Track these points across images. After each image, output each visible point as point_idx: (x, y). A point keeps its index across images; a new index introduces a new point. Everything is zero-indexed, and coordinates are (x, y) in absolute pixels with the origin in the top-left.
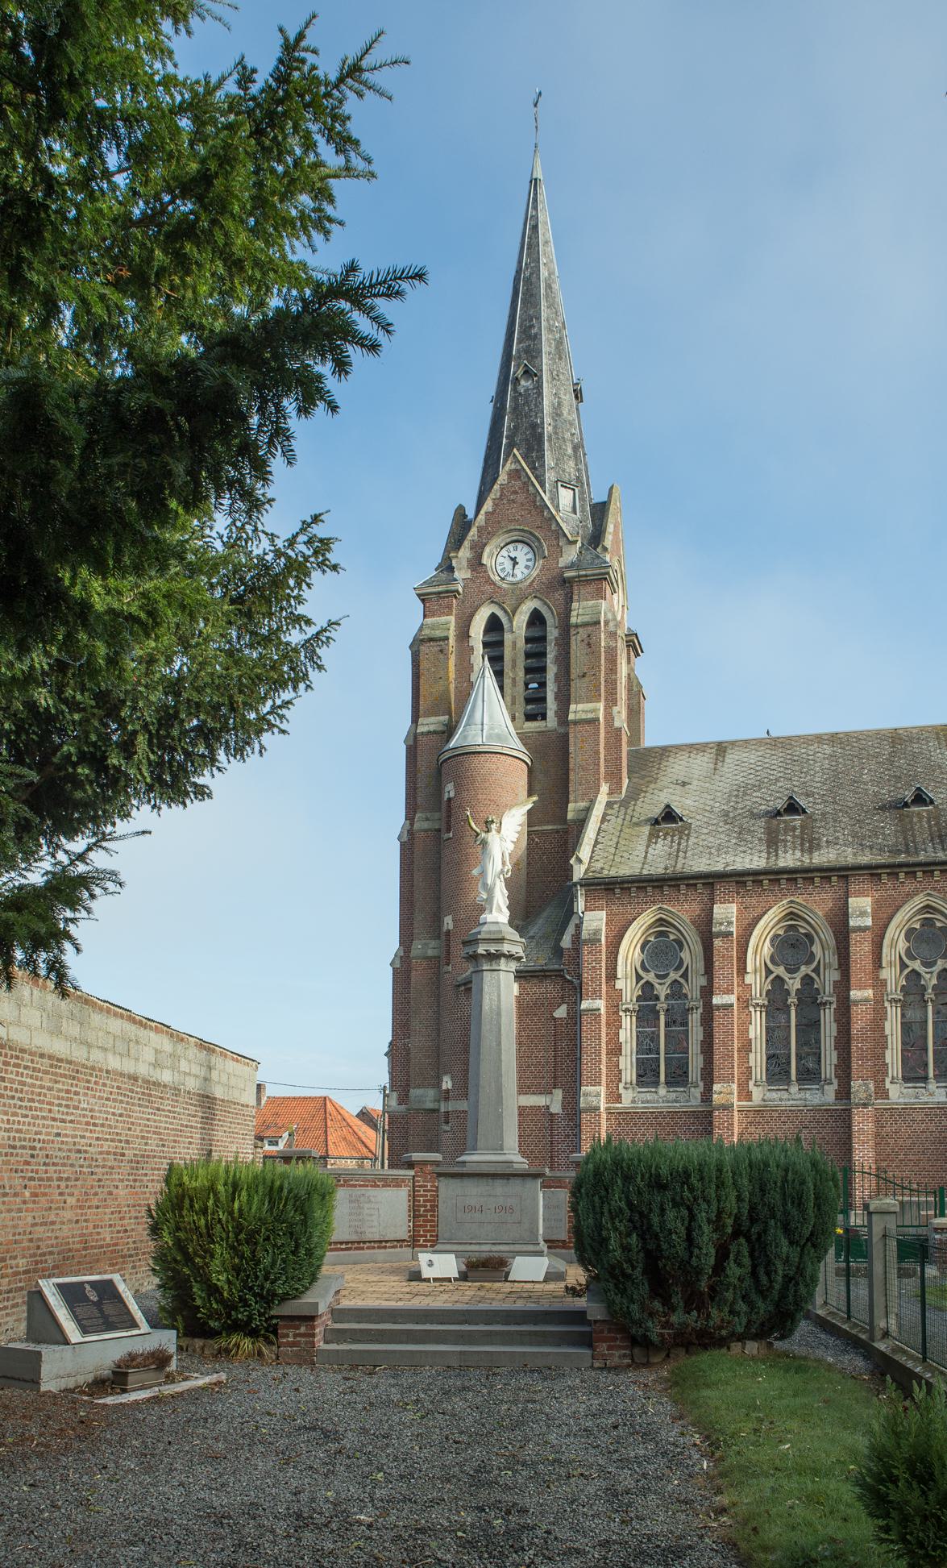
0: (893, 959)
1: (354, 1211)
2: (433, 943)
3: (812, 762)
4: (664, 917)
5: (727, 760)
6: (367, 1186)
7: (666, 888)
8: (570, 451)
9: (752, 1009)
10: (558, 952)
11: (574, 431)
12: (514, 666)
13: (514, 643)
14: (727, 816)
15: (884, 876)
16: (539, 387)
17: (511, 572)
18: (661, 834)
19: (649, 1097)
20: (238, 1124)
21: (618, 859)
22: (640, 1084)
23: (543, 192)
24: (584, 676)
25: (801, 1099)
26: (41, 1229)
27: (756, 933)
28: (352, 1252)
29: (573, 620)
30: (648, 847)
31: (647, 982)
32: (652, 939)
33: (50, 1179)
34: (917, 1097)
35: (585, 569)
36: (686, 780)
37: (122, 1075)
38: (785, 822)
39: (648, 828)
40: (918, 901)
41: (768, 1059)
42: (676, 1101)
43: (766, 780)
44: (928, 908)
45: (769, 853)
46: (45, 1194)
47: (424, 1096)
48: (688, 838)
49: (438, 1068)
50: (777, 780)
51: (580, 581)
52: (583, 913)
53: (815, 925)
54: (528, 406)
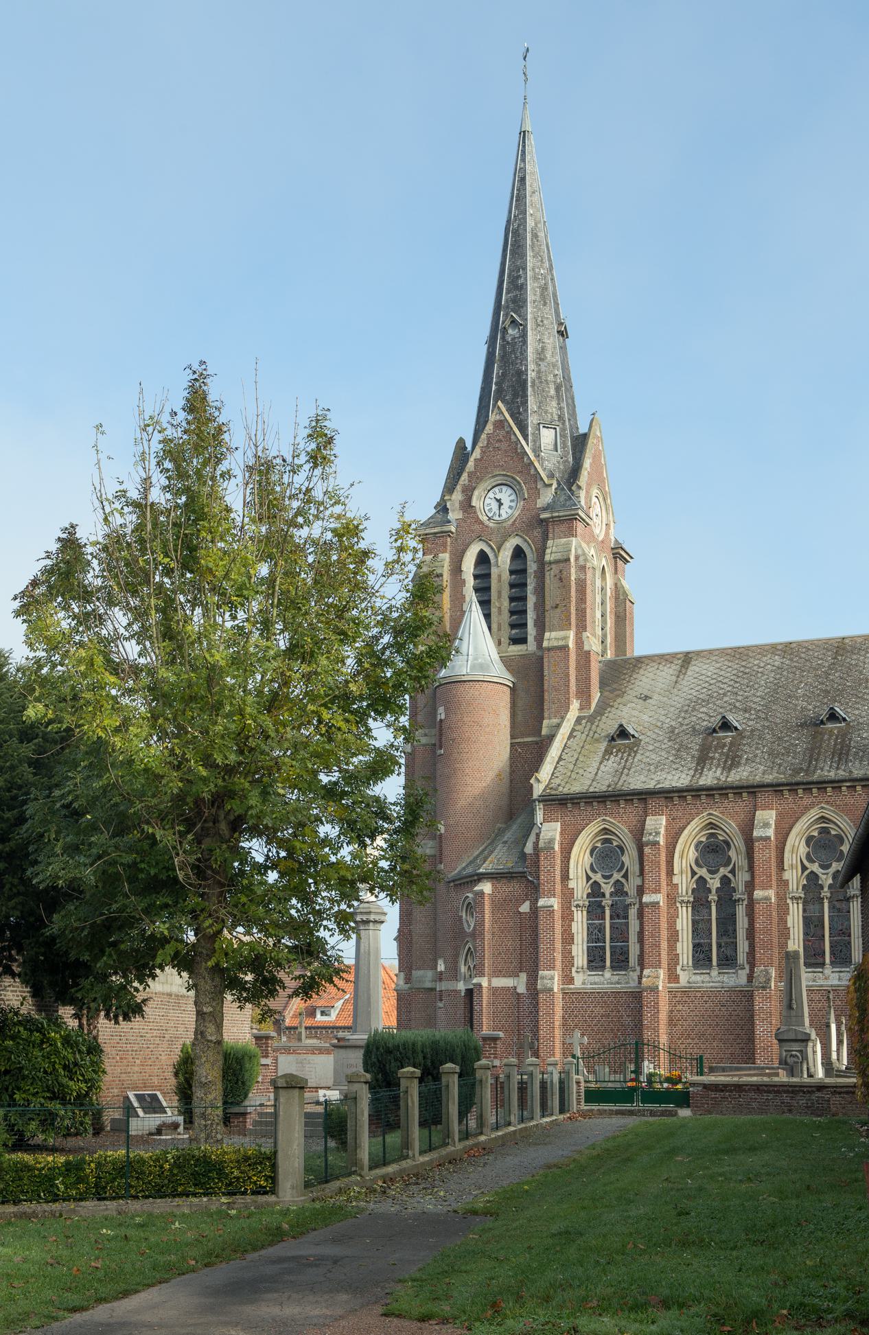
0: (794, 862)
3: (759, 675)
4: (608, 827)
5: (689, 673)
7: (608, 803)
8: (552, 392)
9: (678, 905)
10: (523, 856)
11: (556, 372)
12: (499, 597)
13: (500, 576)
14: (673, 732)
15: (786, 793)
16: (524, 335)
17: (497, 512)
18: (615, 750)
19: (597, 979)
21: (573, 777)
22: (590, 968)
23: (531, 141)
24: (556, 607)
25: (719, 982)
26: (124, 1075)
27: (681, 840)
29: (547, 558)
30: (601, 763)
31: (595, 882)
32: (599, 845)
33: (128, 1051)
34: (814, 981)
35: (558, 511)
36: (649, 694)
37: (163, 994)
38: (719, 738)
39: (605, 744)
40: (814, 813)
41: (694, 947)
42: (618, 983)
43: (715, 694)
44: (823, 819)
45: (696, 770)
46: (126, 1058)
47: (425, 977)
48: (635, 755)
50: (725, 694)
51: (554, 521)
52: (541, 824)
53: (730, 834)
54: (515, 354)
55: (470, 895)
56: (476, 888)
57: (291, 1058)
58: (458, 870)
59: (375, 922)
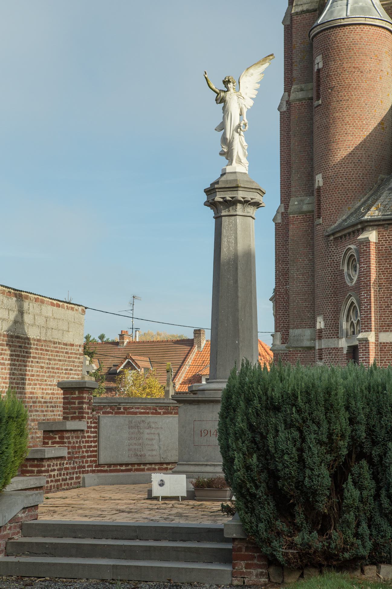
1: (133, 436)
2: (308, 199)
6: (148, 413)
20: (60, 360)
28: (132, 473)
49: (314, 311)
55: (352, 247)
56: (361, 237)
57: (121, 419)
58: (338, 223)
59: (246, 202)
